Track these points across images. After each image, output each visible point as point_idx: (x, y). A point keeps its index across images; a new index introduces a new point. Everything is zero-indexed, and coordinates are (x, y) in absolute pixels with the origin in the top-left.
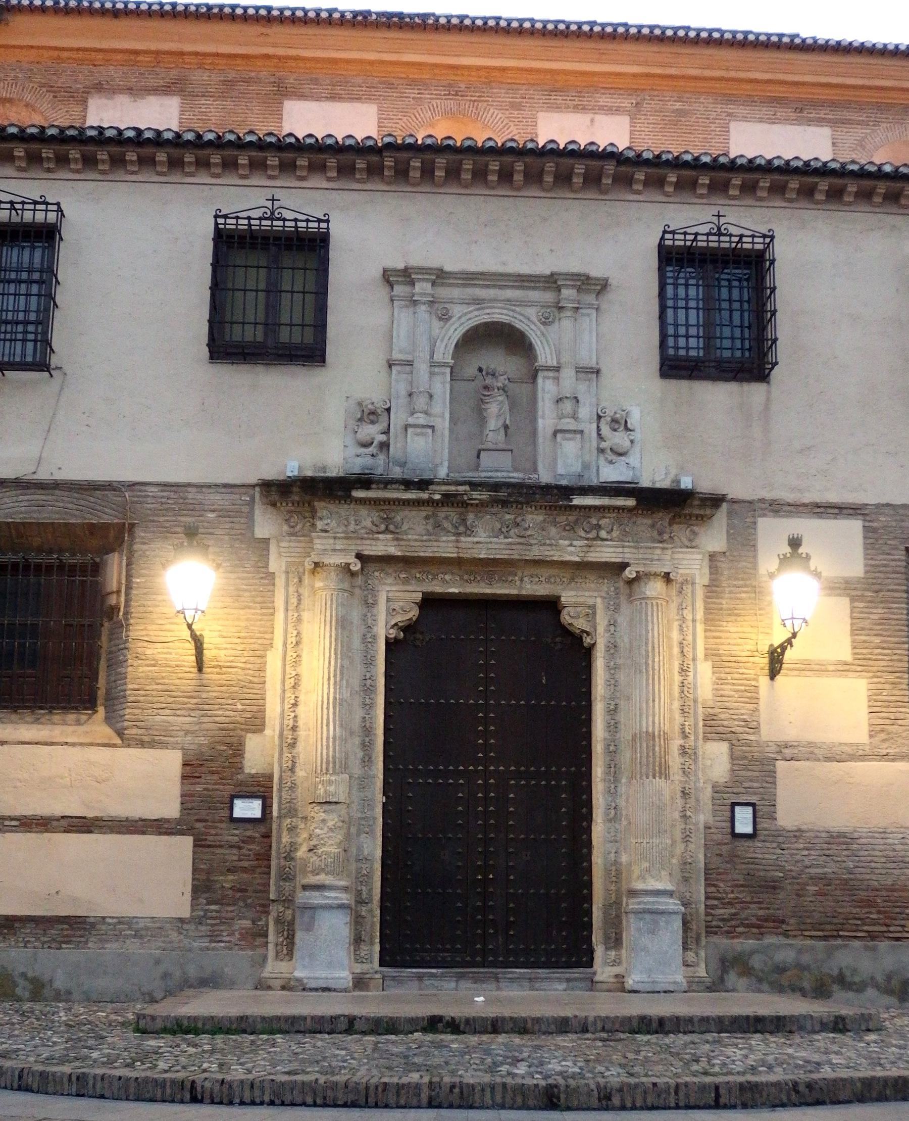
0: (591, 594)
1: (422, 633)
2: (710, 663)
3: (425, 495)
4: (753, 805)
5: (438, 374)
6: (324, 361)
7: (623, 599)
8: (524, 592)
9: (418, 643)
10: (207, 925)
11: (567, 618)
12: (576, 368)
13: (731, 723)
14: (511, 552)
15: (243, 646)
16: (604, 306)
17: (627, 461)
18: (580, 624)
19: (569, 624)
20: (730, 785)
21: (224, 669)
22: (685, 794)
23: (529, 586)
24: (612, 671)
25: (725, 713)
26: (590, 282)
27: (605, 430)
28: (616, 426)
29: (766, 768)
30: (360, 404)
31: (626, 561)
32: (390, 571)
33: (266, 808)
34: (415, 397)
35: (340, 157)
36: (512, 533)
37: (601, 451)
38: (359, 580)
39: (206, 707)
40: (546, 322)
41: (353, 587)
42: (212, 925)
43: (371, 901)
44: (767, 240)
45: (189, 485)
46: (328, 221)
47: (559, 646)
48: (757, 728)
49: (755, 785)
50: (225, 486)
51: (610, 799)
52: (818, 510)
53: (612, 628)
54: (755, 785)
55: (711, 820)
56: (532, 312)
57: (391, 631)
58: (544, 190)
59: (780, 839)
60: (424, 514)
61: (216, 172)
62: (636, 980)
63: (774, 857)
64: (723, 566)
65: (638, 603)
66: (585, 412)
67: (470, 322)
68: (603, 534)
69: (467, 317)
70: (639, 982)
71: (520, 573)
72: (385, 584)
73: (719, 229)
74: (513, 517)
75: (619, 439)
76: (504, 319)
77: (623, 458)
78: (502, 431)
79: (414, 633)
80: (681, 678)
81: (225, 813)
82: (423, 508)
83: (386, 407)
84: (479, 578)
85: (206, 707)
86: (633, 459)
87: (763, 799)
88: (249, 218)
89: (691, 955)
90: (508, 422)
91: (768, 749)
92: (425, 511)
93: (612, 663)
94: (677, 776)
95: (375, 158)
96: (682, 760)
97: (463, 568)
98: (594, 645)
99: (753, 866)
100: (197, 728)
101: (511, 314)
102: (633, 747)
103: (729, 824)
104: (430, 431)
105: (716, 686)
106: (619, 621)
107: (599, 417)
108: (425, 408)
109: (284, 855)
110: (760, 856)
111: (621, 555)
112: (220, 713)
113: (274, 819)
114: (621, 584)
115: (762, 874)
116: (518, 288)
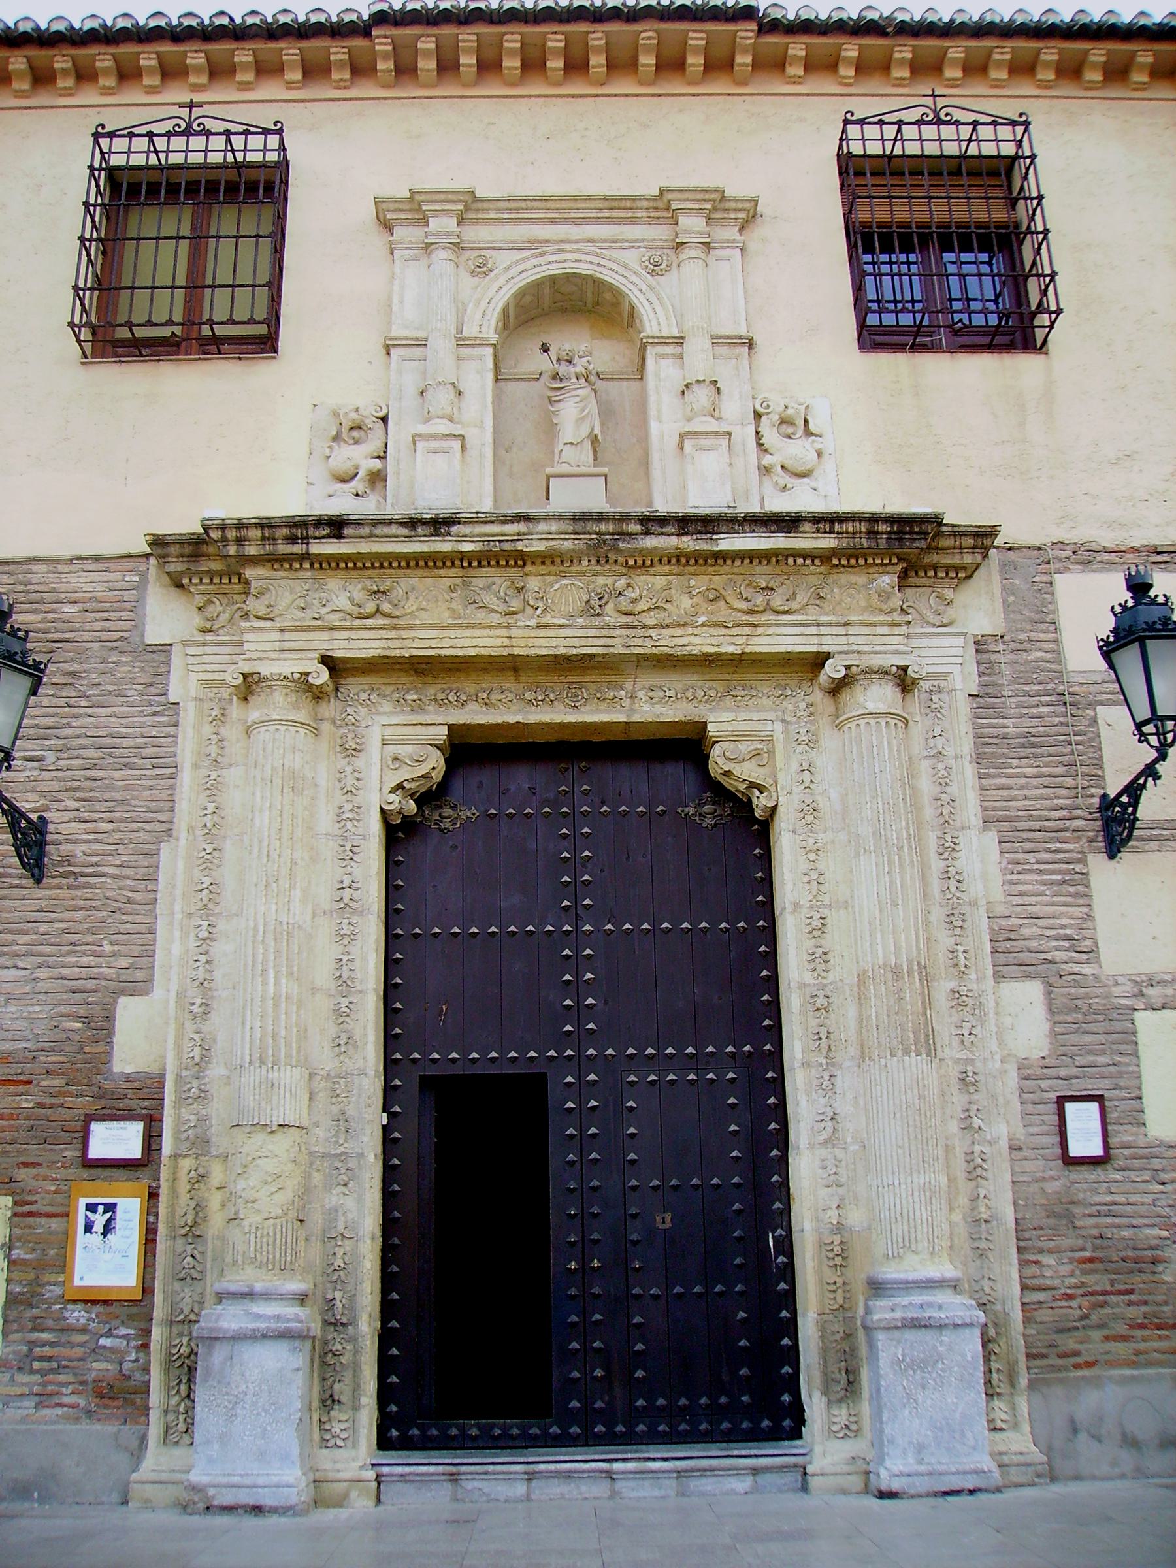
0: (762, 715)
1: (454, 808)
2: (992, 837)
3: (444, 546)
4: (1099, 1099)
5: (471, 358)
6: (275, 350)
7: (824, 722)
8: (636, 718)
9: (447, 824)
10: (32, 1372)
11: (720, 761)
12: (713, 337)
13: (1045, 944)
14: (610, 642)
15: (117, 836)
16: (752, 247)
17: (814, 484)
18: (747, 771)
19: (727, 774)
20: (1047, 1062)
21: (81, 879)
22: (967, 1082)
23: (646, 708)
24: (812, 856)
25: (1031, 925)
26: (728, 205)
27: (770, 436)
28: (790, 430)
29: (1118, 1026)
30: (336, 414)
31: (825, 649)
32: (388, 690)
33: (151, 1140)
34: (429, 395)
35: (305, 44)
36: (609, 608)
37: (765, 471)
38: (329, 709)
39: (47, 949)
40: (655, 269)
41: (318, 719)
42: (43, 1373)
43: (353, 1322)
44: (1020, 130)
45: (35, 560)
46: (280, 132)
47: (709, 821)
48: (1092, 953)
49: (1101, 1060)
50: (97, 559)
51: (823, 1101)
52: (1160, 558)
53: (806, 776)
54: (1101, 1060)
55: (1020, 1133)
56: (631, 257)
57: (392, 797)
58: (641, 83)
59: (1156, 1164)
60: (447, 582)
61: (107, 84)
62: (896, 1470)
63: (1148, 1199)
64: (1001, 658)
65: (852, 725)
66: (735, 408)
67: (524, 275)
68: (777, 601)
69: (521, 267)
70: (901, 1475)
71: (629, 686)
72: (379, 714)
73: (937, 114)
74: (609, 581)
75: (798, 451)
76: (583, 269)
77: (805, 480)
78: (587, 445)
79: (441, 807)
80: (943, 864)
81: (72, 1153)
82: (442, 572)
83: (381, 414)
84: (552, 697)
85: (47, 949)
86: (827, 472)
87: (1117, 1087)
88: (150, 135)
89: (1000, 1407)
90: (597, 431)
91: (1116, 991)
92: (449, 578)
93: (811, 841)
94: (951, 1051)
95: (358, 42)
96: (955, 1018)
97: (522, 679)
98: (775, 808)
99: (1109, 1220)
100: (27, 989)
101: (595, 260)
102: (861, 999)
103: (1057, 1139)
104: (456, 445)
105: (1009, 877)
106: (818, 763)
107: (758, 416)
108: (449, 411)
109: (183, 1231)
110: (1121, 1199)
111: (815, 640)
112: (72, 959)
113: (164, 1160)
114: (818, 696)
115: (1125, 1233)
116: (610, 220)
